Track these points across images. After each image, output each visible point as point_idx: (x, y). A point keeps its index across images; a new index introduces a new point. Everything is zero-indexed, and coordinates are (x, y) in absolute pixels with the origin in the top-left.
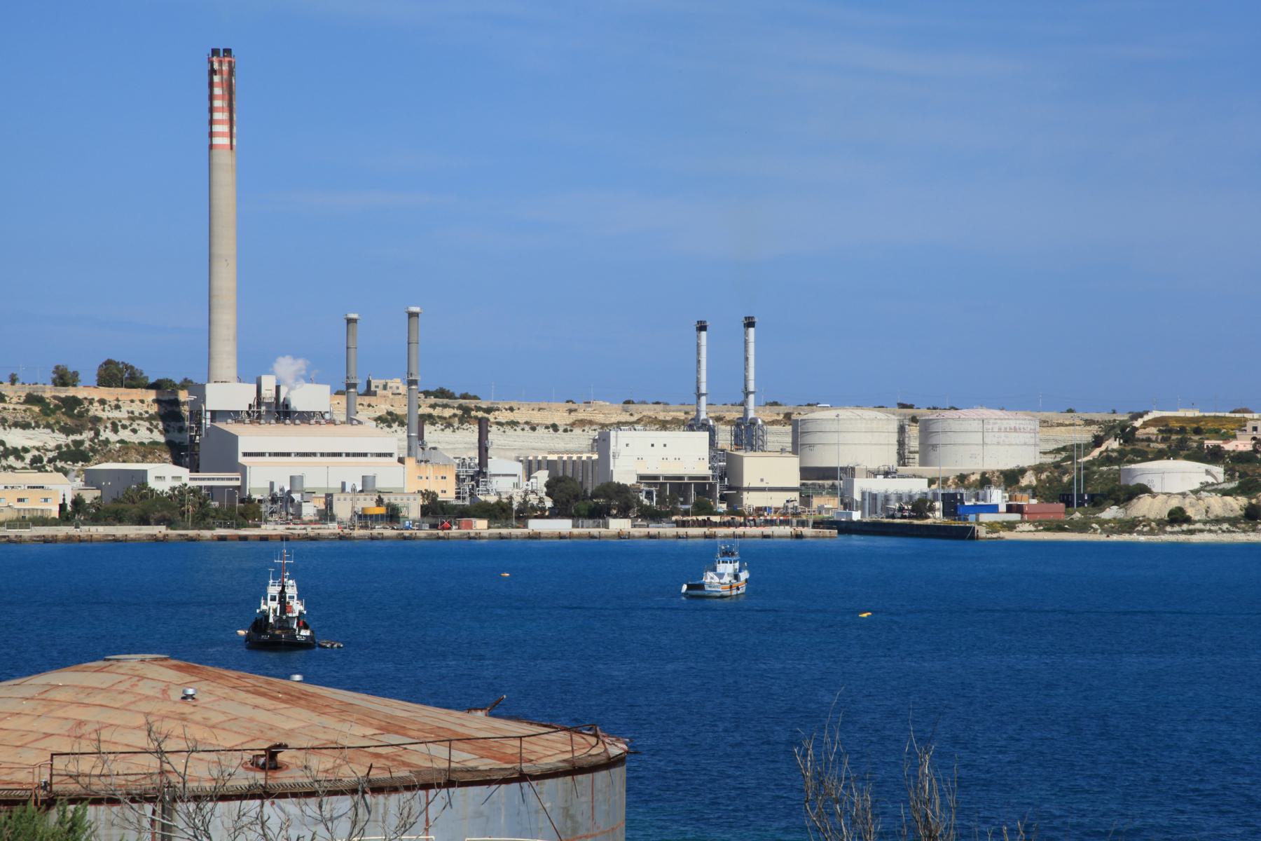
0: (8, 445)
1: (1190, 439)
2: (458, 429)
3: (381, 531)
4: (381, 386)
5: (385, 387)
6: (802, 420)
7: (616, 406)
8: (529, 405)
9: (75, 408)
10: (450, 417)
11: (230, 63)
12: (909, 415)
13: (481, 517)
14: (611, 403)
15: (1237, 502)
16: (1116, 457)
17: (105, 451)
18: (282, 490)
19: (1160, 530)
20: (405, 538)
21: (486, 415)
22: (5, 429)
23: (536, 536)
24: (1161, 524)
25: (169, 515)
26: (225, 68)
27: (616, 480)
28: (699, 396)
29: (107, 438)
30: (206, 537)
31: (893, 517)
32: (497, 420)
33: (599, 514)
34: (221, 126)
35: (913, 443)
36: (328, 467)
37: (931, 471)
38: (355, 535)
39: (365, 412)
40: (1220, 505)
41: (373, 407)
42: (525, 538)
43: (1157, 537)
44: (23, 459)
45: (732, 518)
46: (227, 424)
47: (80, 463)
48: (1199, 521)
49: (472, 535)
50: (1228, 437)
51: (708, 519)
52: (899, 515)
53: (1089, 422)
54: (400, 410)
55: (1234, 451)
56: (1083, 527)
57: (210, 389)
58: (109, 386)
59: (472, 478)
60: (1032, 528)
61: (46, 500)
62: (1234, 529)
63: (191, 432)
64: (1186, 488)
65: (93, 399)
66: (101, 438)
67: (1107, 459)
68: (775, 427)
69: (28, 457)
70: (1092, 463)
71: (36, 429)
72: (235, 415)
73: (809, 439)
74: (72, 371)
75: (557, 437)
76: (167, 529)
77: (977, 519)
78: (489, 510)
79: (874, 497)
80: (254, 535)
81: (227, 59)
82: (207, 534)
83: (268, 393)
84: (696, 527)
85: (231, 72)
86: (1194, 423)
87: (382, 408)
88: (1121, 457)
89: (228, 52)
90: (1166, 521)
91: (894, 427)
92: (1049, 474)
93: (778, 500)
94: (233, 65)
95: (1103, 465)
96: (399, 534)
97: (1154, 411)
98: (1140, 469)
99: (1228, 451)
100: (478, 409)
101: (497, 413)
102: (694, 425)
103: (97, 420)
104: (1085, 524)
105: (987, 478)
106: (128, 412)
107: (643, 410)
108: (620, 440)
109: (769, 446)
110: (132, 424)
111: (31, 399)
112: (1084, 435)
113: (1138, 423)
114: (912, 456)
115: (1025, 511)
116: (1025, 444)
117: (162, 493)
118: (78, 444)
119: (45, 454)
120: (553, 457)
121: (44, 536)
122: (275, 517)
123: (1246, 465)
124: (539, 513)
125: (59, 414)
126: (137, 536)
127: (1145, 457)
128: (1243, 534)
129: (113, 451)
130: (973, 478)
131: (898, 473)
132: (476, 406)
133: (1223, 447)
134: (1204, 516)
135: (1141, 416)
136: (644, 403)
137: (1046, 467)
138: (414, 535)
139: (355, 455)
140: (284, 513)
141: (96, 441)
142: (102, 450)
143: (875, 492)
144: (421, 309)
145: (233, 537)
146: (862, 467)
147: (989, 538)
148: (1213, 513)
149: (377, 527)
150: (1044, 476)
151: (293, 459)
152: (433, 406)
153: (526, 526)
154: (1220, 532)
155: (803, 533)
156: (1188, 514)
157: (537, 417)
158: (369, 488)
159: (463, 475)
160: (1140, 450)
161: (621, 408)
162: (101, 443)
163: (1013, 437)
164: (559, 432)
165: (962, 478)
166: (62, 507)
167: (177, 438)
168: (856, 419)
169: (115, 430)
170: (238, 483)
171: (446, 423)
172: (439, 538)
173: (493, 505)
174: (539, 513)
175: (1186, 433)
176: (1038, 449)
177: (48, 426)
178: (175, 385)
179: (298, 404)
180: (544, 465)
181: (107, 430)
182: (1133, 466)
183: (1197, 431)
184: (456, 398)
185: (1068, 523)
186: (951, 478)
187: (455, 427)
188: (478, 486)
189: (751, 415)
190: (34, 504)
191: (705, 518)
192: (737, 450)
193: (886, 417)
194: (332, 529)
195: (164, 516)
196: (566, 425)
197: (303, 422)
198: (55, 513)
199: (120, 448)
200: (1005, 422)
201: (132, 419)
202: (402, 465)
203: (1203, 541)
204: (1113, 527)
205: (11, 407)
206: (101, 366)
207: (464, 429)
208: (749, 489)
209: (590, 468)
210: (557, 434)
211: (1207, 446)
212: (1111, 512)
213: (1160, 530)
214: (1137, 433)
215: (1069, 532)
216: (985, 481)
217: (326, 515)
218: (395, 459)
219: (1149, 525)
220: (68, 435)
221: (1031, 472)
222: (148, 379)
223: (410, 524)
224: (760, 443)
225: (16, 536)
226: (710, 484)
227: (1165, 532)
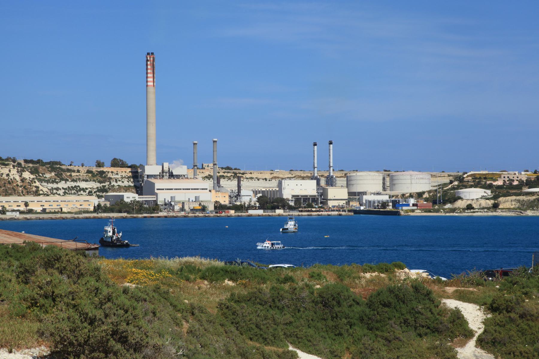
0: (81, 187)
2: (233, 180)
3: (198, 214)
4: (207, 166)
5: (208, 166)
7: (287, 172)
10: (230, 176)
11: (153, 57)
13: (232, 209)
16: (456, 188)
18: (168, 201)
20: (206, 216)
21: (242, 175)
22: (80, 182)
23: (251, 216)
24: (464, 210)
26: (152, 59)
27: (284, 198)
28: (314, 168)
31: (375, 208)
33: (274, 208)
35: (388, 184)
37: (393, 193)
39: (201, 175)
40: (484, 203)
44: (86, 192)
47: (105, 193)
48: (477, 209)
49: (229, 215)
50: (495, 180)
52: (377, 207)
53: (449, 176)
54: (212, 174)
55: (497, 185)
56: (437, 211)
57: (146, 167)
59: (236, 197)
60: (420, 211)
64: (475, 198)
66: (112, 185)
67: (453, 188)
68: (341, 178)
69: (87, 191)
72: (155, 176)
73: (352, 182)
77: (402, 209)
79: (370, 202)
81: (152, 56)
82: (140, 216)
83: (166, 169)
86: (484, 175)
87: (207, 173)
88: (458, 187)
89: (152, 54)
91: (381, 178)
93: (342, 203)
99: (495, 185)
101: (246, 175)
102: (312, 178)
103: (110, 178)
105: (412, 195)
108: (285, 183)
109: (337, 185)
112: (447, 180)
113: (465, 176)
114: (387, 188)
116: (426, 183)
117: (128, 202)
118: (104, 186)
120: (264, 189)
122: (166, 210)
123: (500, 190)
125: (98, 177)
127: (466, 187)
130: (407, 195)
135: (467, 173)
139: (194, 189)
140: (169, 209)
143: (370, 200)
150: (431, 194)
151: (173, 191)
152: (224, 173)
157: (260, 176)
158: (197, 200)
163: (421, 181)
165: (403, 195)
166: (94, 207)
167: (138, 184)
169: (116, 182)
170: (155, 199)
172: (218, 216)
176: (430, 185)
177: (94, 181)
178: (137, 166)
180: (261, 192)
183: (485, 178)
184: (232, 170)
185: (432, 210)
186: (400, 195)
188: (237, 200)
189: (332, 174)
190: (85, 206)
191: (310, 209)
192: (327, 186)
194: (183, 213)
197: (177, 178)
198: (92, 209)
201: (122, 178)
205: (82, 174)
210: (267, 182)
212: (448, 206)
217: (183, 209)
218: (208, 190)
220: (100, 184)
224: (335, 184)
227: (465, 212)
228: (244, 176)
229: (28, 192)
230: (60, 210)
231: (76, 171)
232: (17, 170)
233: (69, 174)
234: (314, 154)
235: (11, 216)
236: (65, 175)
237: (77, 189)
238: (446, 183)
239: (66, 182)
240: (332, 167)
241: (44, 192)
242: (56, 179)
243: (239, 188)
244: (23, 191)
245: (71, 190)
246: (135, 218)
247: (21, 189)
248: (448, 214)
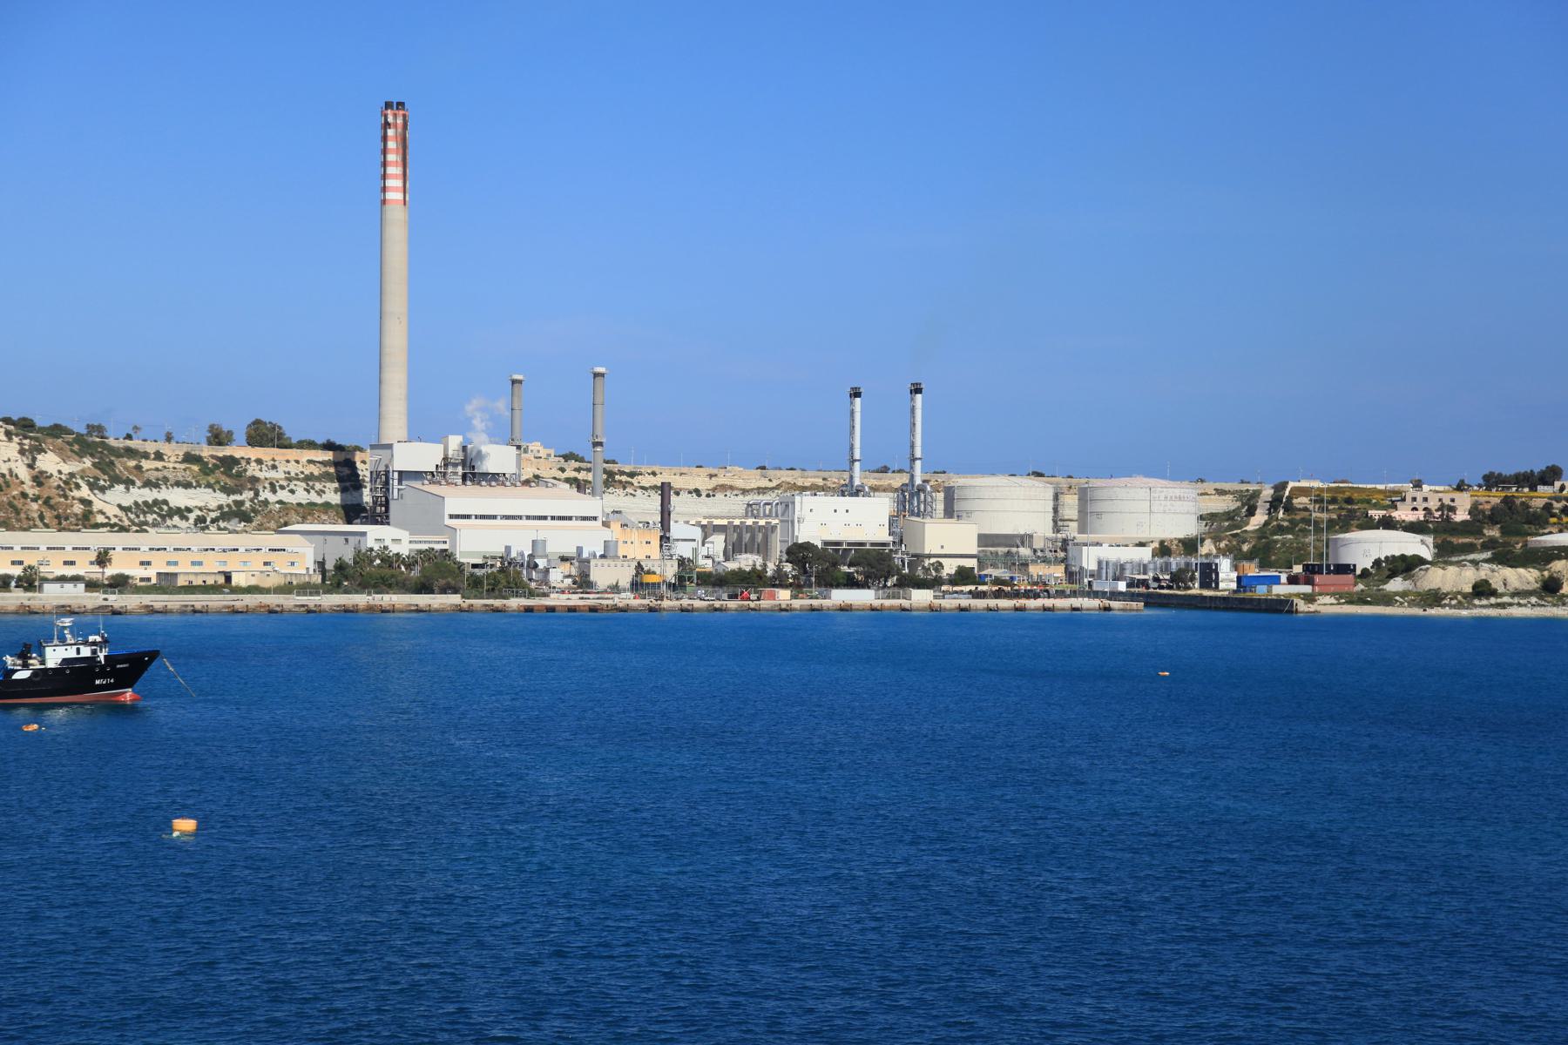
0: (171, 505)
11: (404, 116)
20: (716, 610)
21: (629, 479)
22: (168, 488)
23: (845, 609)
26: (400, 121)
28: (853, 461)
29: (266, 499)
31: (1161, 587)
34: (395, 181)
44: (187, 519)
61: (293, 564)
65: (250, 459)
66: (260, 499)
69: (192, 516)
71: (198, 488)
81: (401, 112)
89: (401, 105)
91: (1050, 494)
96: (710, 605)
100: (622, 473)
103: (254, 480)
106: (285, 473)
107: (782, 476)
108: (806, 505)
111: (189, 458)
116: (1188, 513)
118: (239, 504)
120: (725, 522)
121: (344, 606)
125: (218, 474)
131: (1075, 541)
132: (619, 471)
141: (256, 501)
146: (1039, 534)
147: (1307, 612)
158: (611, 553)
163: (1178, 506)
169: (274, 491)
177: (209, 486)
179: (489, 466)
195: (448, 583)
199: (280, 508)
201: (289, 479)
204: (1414, 600)
205: (171, 465)
206: (249, 426)
215: (1374, 605)
217: (583, 582)
218: (599, 523)
220: (228, 495)
225: (316, 605)
227: (1476, 606)
228: (634, 481)
229: (58, 517)
230: (221, 580)
231: (153, 456)
232: (18, 447)
233: (132, 463)
235: (61, 598)
236: (125, 465)
237: (162, 510)
238: (1214, 511)
239: (128, 489)
240: (858, 460)
241: (108, 518)
242: (99, 480)
243: (666, 514)
244: (42, 513)
245: (145, 513)
246: (497, 610)
247: (35, 506)
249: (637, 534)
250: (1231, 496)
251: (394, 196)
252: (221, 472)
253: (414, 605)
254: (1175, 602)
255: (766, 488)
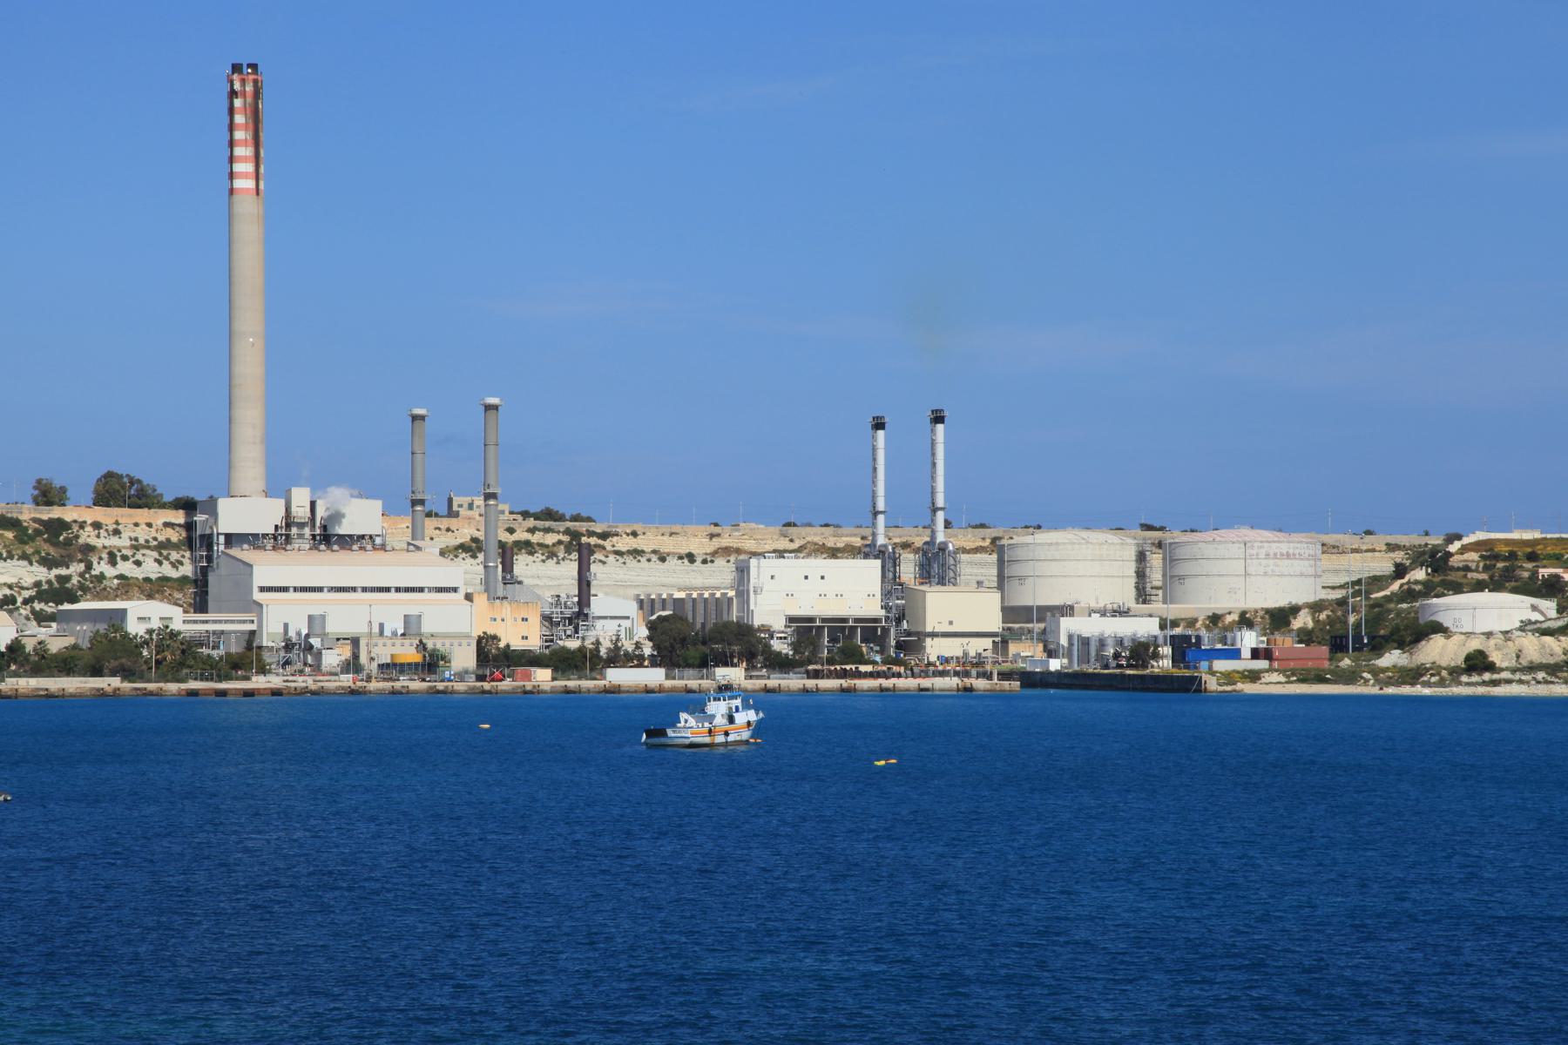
1: (1521, 567)
2: (563, 559)
3: (406, 684)
4: (466, 506)
6: (1008, 545)
7: (771, 529)
8: (657, 528)
9: (61, 534)
10: (554, 545)
11: (255, 82)
12: (1150, 539)
14: (766, 526)
15: (1559, 643)
16: (1420, 592)
17: (98, 589)
18: (299, 634)
19: (1453, 680)
20: (439, 692)
21: (600, 542)
23: (615, 690)
24: (1455, 672)
25: (129, 663)
26: (249, 88)
30: (171, 691)
31: (1106, 667)
32: (615, 549)
35: (1156, 577)
36: (370, 606)
37: (1174, 611)
38: (372, 689)
40: (1534, 648)
41: (453, 532)
42: (600, 692)
43: (1447, 689)
45: (889, 668)
46: (242, 550)
48: (1507, 669)
51: (857, 668)
53: (1391, 548)
56: (1351, 677)
58: (108, 506)
60: (1282, 679)
62: (1553, 679)
63: (200, 562)
64: (1498, 626)
65: (85, 522)
66: (93, 573)
67: (1409, 594)
70: (1388, 599)
71: (9, 561)
72: (253, 540)
74: (58, 486)
75: (693, 571)
76: (122, 682)
77: (1210, 667)
78: (568, 658)
79: (1085, 642)
80: (236, 689)
82: (173, 687)
83: (301, 511)
84: (834, 678)
85: (257, 94)
88: (1429, 589)
89: (254, 66)
90: (1462, 668)
91: (1131, 553)
92: (1330, 613)
94: (260, 84)
95: (1403, 601)
96: (431, 688)
97: (1477, 532)
98: (1444, 604)
100: (591, 534)
102: (868, 551)
103: (89, 549)
104: (1353, 672)
106: (131, 539)
108: (760, 570)
109: (962, 579)
110: (135, 553)
112: (1383, 565)
113: (1454, 547)
114: (1154, 592)
115: (1274, 657)
116: (1302, 575)
119: (20, 594)
124: (636, 662)
125: (39, 542)
126: (79, 691)
127: (1457, 589)
128: (1564, 686)
129: (108, 589)
130: (1229, 619)
132: (587, 531)
133: (1563, 578)
134: (1514, 661)
135: (1459, 537)
136: (809, 525)
137: (1327, 604)
138: (450, 688)
139: (408, 590)
141: (87, 576)
142: (95, 588)
144: (501, 400)
145: (207, 692)
146: (1082, 605)
147: (1220, 692)
148: (1526, 657)
149: (401, 678)
150: (1323, 616)
152: (532, 531)
153: (604, 678)
154: (1534, 682)
155: (974, 686)
156: (1491, 659)
157: (667, 544)
158: (413, 630)
159: (557, 618)
160: (1453, 581)
161: (778, 532)
162: (94, 579)
164: (695, 564)
168: (1079, 544)
169: (113, 562)
170: (253, 627)
171: (549, 552)
172: (484, 692)
173: (574, 652)
174: (636, 662)
175: (1516, 559)
177: (24, 557)
181: (102, 562)
182: (1435, 600)
183: (1532, 557)
185: (1331, 672)
186: (1201, 618)
187: (560, 558)
192: (922, 584)
193: (1120, 541)
195: (122, 665)
196: (706, 554)
197: (342, 548)
199: (118, 585)
200: (1274, 545)
201: (136, 548)
202: (470, 603)
203: (1508, 694)
204: (1390, 678)
206: (99, 480)
207: (571, 560)
208: (934, 635)
209: (725, 607)
211: (1543, 576)
212: (1392, 658)
213: (1453, 680)
214: (1451, 559)
216: (1245, 621)
218: (460, 596)
219: (1439, 674)
220: (50, 569)
221: (1307, 610)
222: (162, 498)
223: (450, 675)
224: (952, 574)
226: (883, 628)
227: (1460, 683)
228: (607, 544)
234: (933, 454)
238: (1378, 574)
248: (1391, 690)
249: (509, 609)
250: (1403, 553)
251: (244, 184)
252: (44, 540)
253: (42, 689)
254: (1097, 683)
255: (786, 551)
